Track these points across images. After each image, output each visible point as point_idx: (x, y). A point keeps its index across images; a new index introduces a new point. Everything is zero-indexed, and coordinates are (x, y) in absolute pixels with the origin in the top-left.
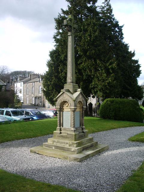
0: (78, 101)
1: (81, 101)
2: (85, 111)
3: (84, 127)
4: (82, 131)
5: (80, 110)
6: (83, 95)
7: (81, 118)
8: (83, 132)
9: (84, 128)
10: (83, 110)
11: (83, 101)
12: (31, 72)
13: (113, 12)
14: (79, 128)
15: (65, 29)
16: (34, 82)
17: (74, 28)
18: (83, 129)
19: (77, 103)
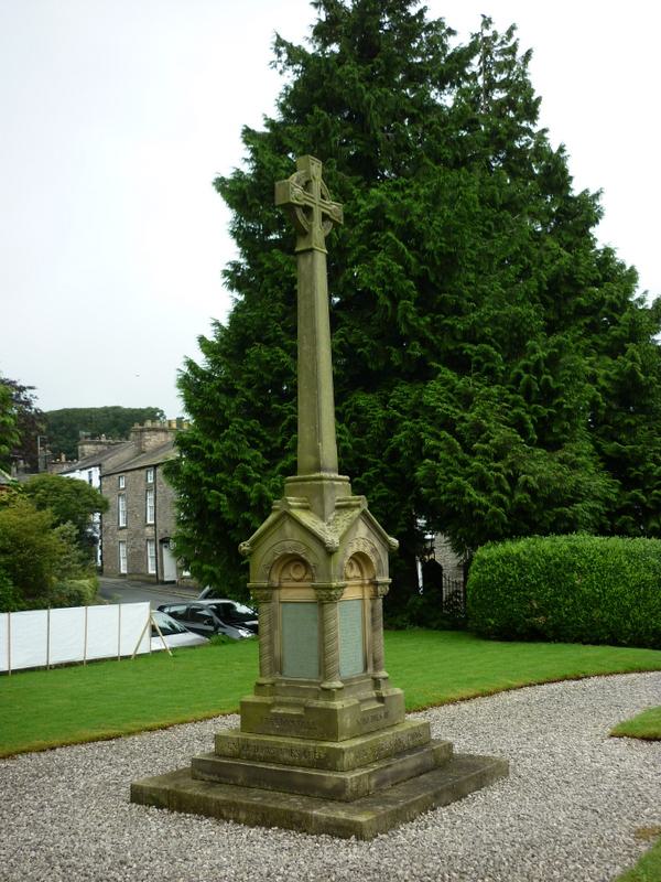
0: (350, 554)
1: (367, 550)
2: (384, 599)
3: (383, 674)
4: (374, 695)
5: (363, 592)
6: (380, 533)
7: (368, 631)
8: (380, 699)
9: (385, 679)
10: (374, 598)
11: (374, 550)
12: (219, 190)
13: (572, 167)
14: (359, 678)
15: (560, 861)
16: (155, 466)
17: (325, 217)
18: (376, 683)
19: (346, 562)
